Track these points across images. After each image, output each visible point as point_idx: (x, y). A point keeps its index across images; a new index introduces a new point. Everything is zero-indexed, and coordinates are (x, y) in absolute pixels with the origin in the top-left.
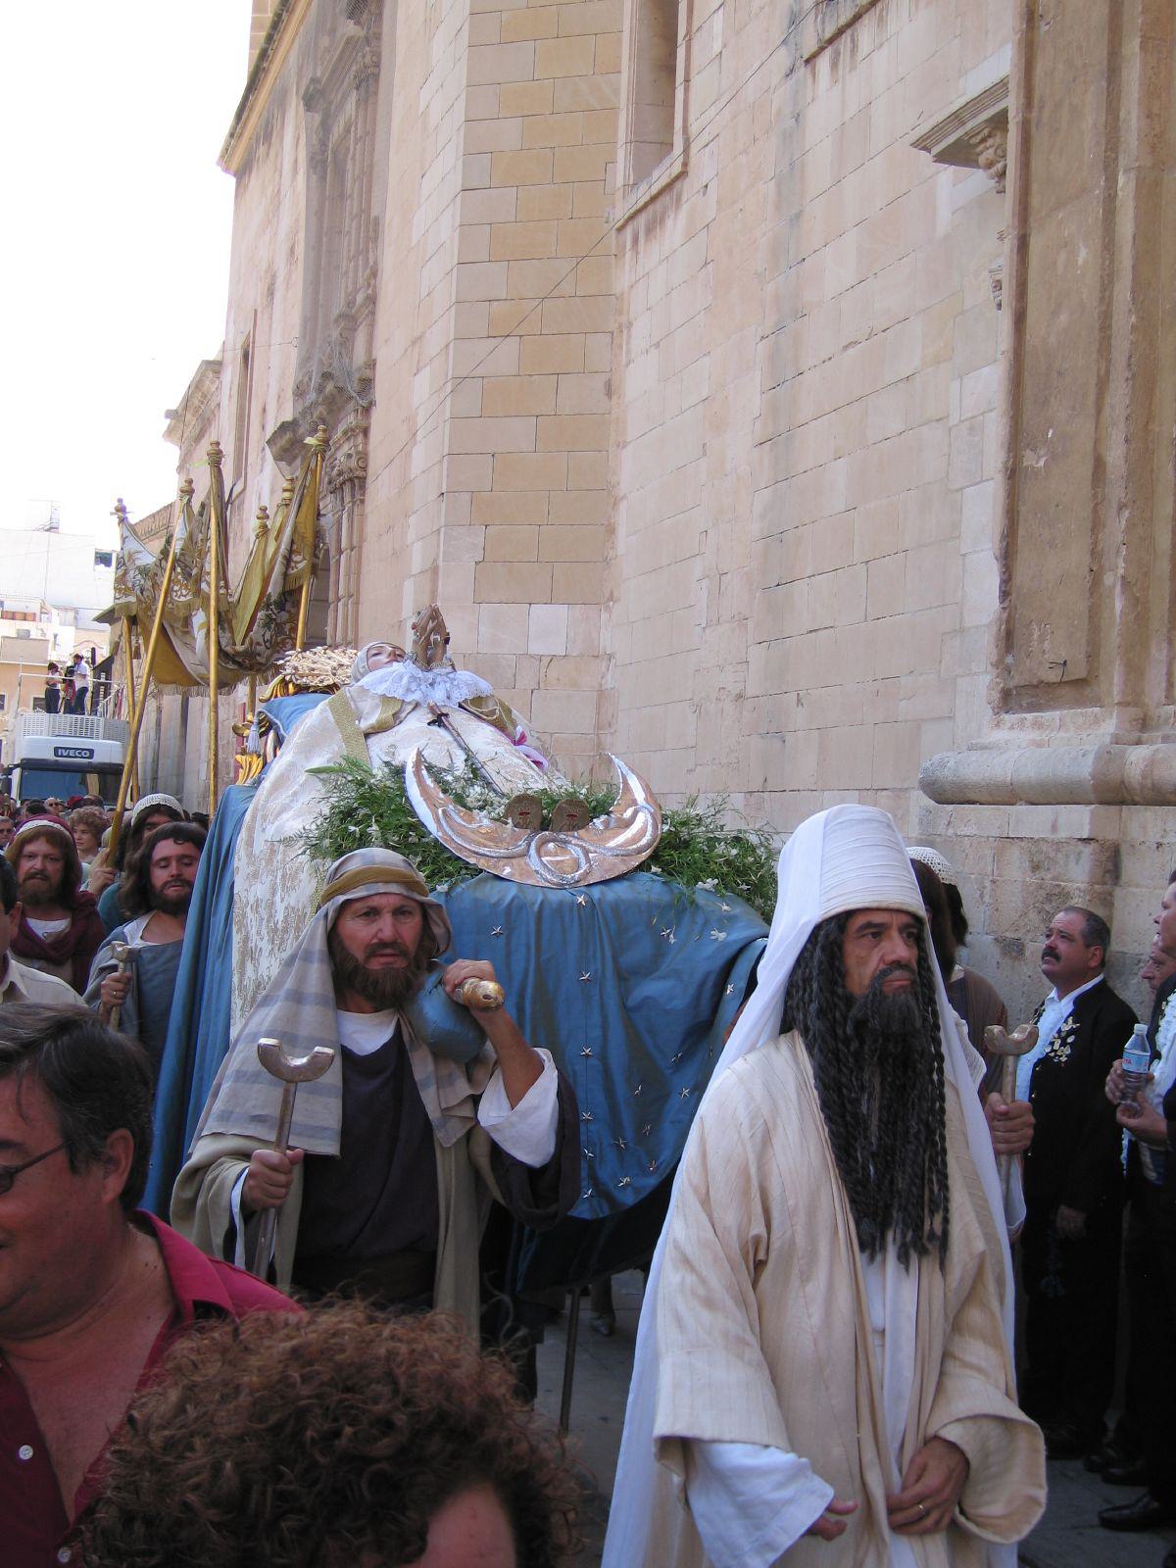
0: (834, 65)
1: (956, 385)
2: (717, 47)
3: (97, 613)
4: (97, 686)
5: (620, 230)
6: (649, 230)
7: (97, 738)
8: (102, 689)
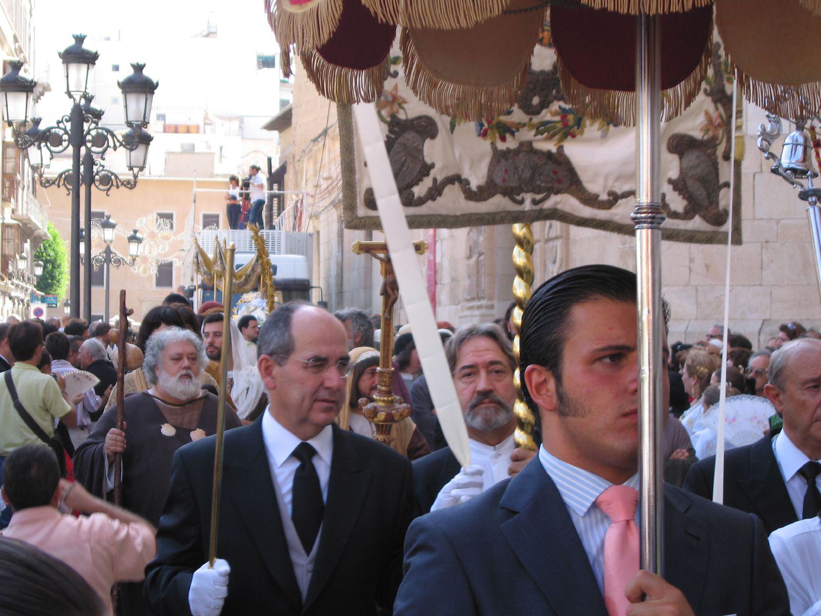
3: (267, 120)
4: (271, 197)
7: (279, 253)
8: (275, 201)
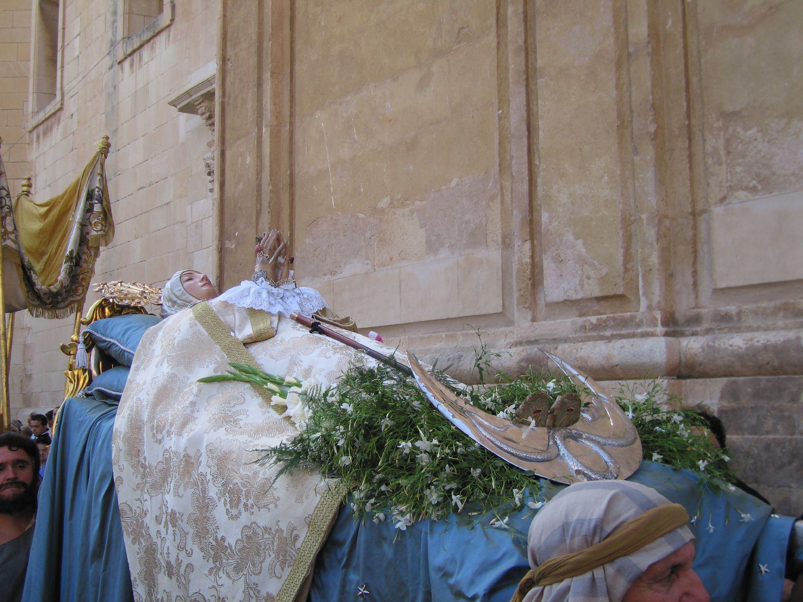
0: (132, 65)
1: (189, 207)
2: (77, 53)
5: (31, 132)
6: (45, 134)
